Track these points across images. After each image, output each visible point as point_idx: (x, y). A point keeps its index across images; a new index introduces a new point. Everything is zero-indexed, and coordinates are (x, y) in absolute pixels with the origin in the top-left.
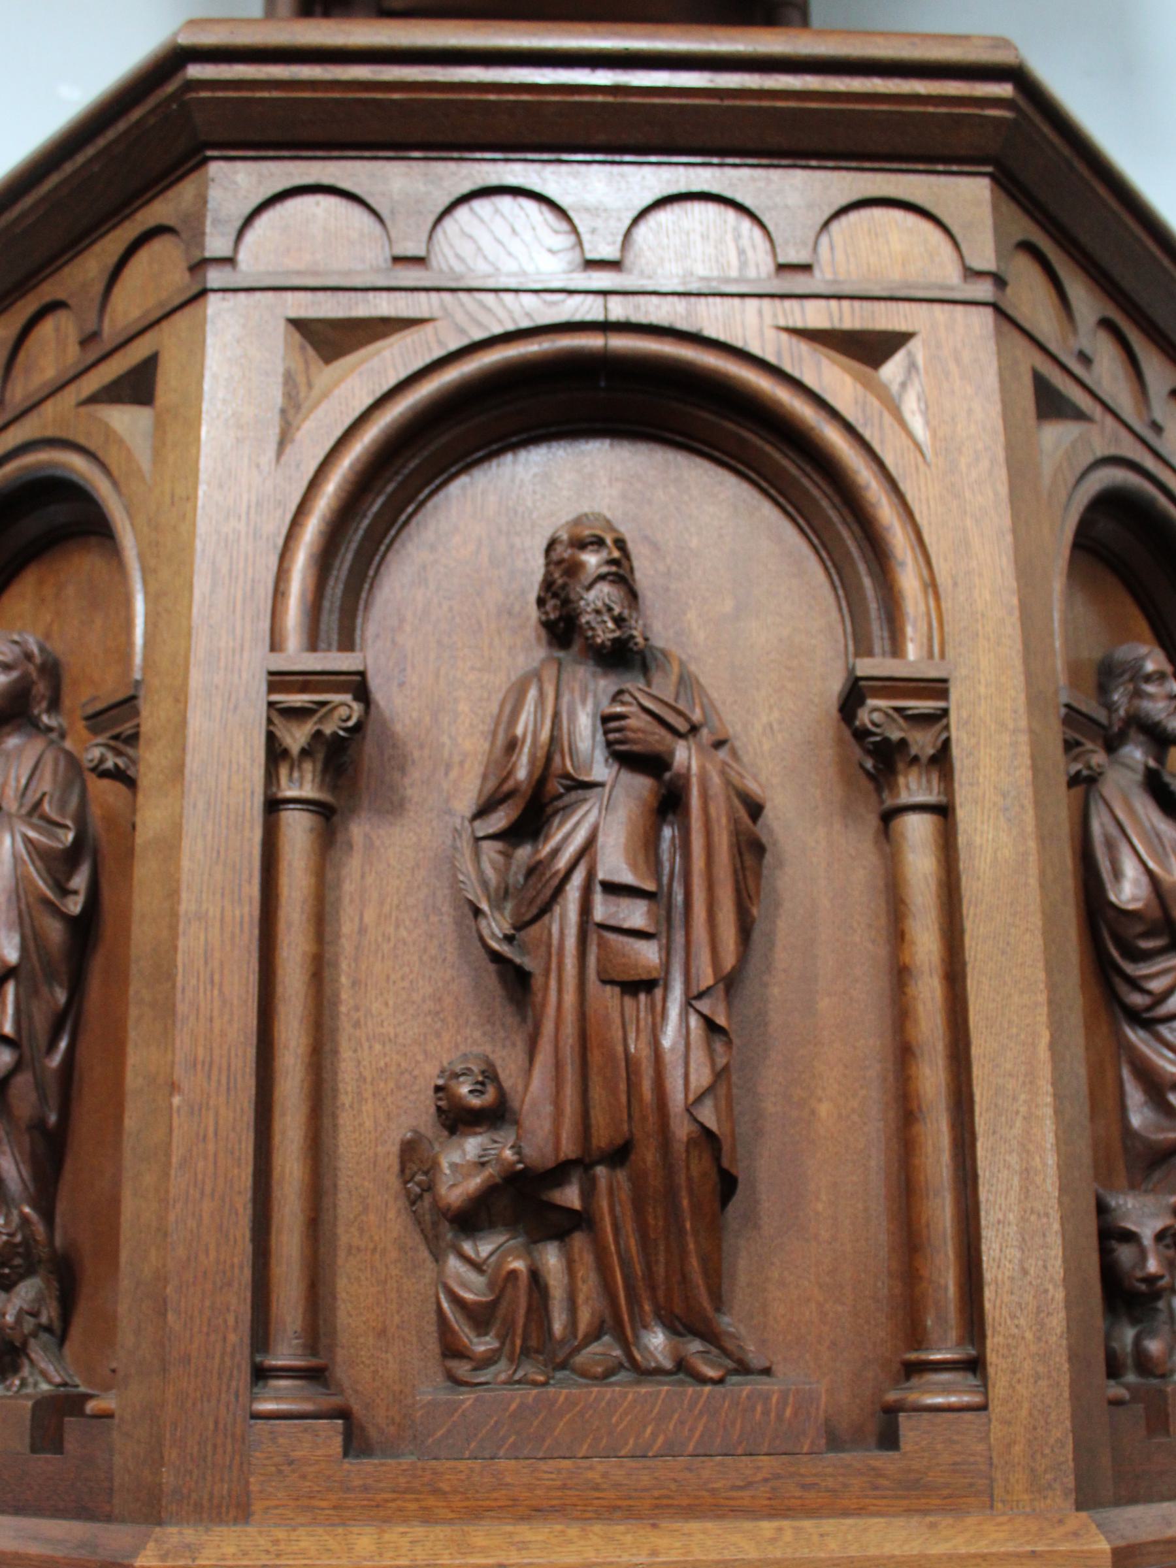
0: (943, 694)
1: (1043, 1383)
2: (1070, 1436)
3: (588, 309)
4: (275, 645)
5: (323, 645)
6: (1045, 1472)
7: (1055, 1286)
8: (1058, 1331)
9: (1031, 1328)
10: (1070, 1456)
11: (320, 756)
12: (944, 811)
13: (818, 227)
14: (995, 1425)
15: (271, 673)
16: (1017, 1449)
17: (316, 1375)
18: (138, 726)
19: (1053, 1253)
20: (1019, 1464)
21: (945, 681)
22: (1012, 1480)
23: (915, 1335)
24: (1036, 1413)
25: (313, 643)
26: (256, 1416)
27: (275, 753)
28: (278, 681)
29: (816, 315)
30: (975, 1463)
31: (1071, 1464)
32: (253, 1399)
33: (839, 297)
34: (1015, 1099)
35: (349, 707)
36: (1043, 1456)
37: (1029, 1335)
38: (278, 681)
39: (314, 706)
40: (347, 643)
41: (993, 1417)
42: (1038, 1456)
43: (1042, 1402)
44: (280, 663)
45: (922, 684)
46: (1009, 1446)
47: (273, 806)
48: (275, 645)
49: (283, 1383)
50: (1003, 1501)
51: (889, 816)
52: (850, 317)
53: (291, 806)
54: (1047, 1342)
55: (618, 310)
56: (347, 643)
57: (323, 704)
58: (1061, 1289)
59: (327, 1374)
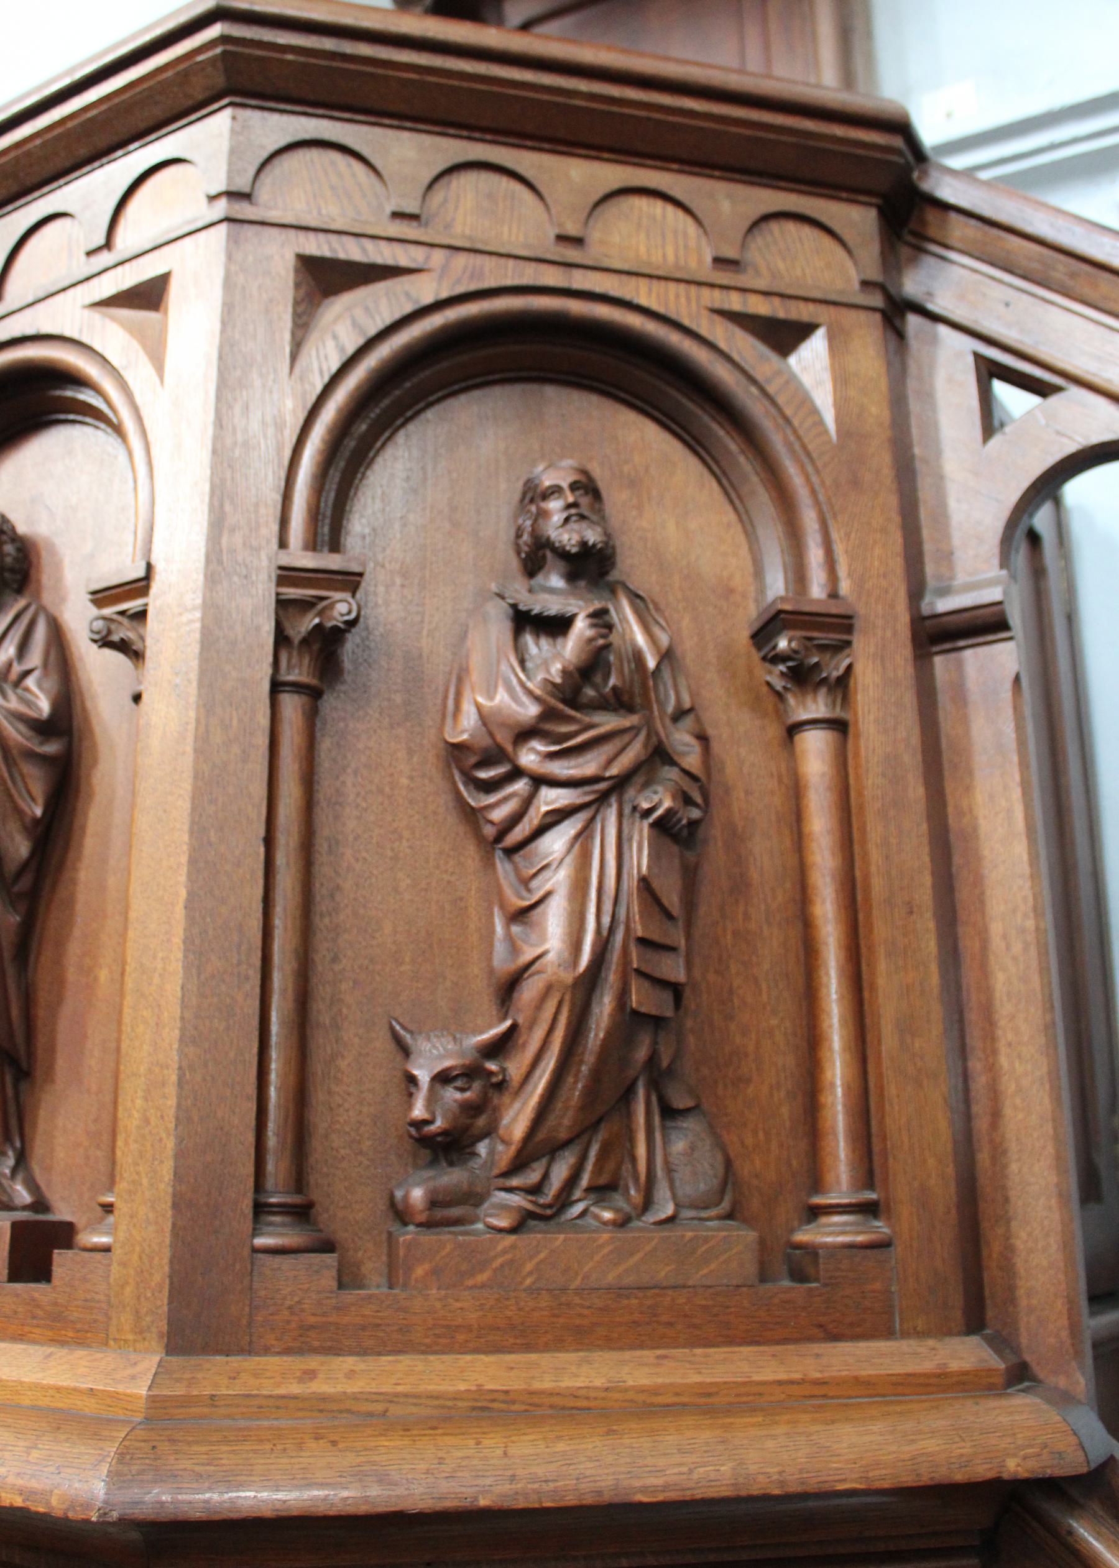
0: (849, 629)
1: (151, 1228)
2: (167, 1281)
3: (551, 277)
4: (283, 544)
5: (319, 548)
6: (147, 1314)
7: (168, 1135)
8: (166, 1179)
9: (147, 1175)
10: (166, 1301)
11: (316, 647)
12: (840, 726)
13: (587, 210)
14: (115, 1268)
15: (281, 568)
16: (128, 1290)
17: (302, 1213)
18: (146, 605)
19: (169, 1103)
20: (128, 1304)
21: (850, 617)
22: (123, 1319)
23: (817, 1183)
24: (144, 1257)
25: (312, 544)
26: (255, 1250)
27: (281, 639)
28: (287, 576)
29: (735, 302)
30: (99, 1302)
31: (166, 1308)
32: (255, 1233)
33: (688, 282)
34: (155, 957)
35: (349, 603)
36: (147, 1299)
37: (145, 1181)
38: (287, 576)
39: (314, 600)
40: (335, 546)
41: (114, 1258)
42: (142, 1299)
43: (150, 1246)
44: (285, 559)
45: (807, 618)
46: (123, 1287)
47: (277, 687)
48: (283, 544)
49: (836, 1219)
50: (115, 1340)
51: (794, 730)
52: (760, 307)
53: (287, 689)
54: (157, 1189)
55: (581, 281)
56: (335, 546)
57: (322, 599)
58: (172, 1138)
59: (313, 1211)
